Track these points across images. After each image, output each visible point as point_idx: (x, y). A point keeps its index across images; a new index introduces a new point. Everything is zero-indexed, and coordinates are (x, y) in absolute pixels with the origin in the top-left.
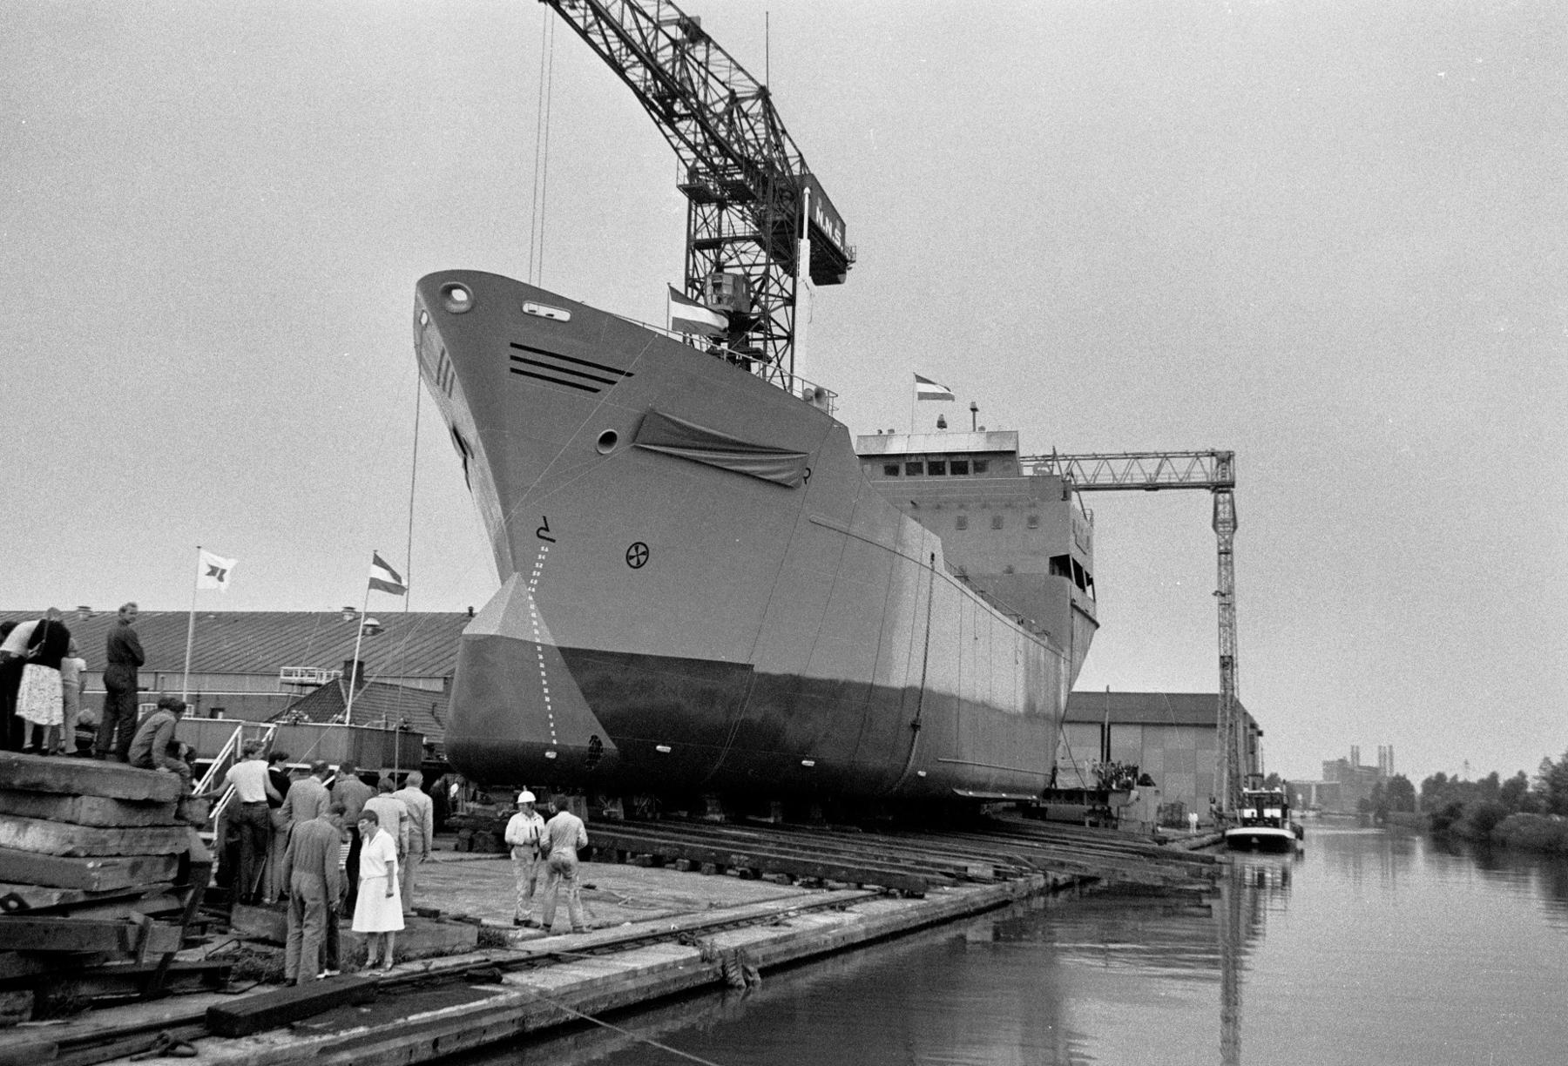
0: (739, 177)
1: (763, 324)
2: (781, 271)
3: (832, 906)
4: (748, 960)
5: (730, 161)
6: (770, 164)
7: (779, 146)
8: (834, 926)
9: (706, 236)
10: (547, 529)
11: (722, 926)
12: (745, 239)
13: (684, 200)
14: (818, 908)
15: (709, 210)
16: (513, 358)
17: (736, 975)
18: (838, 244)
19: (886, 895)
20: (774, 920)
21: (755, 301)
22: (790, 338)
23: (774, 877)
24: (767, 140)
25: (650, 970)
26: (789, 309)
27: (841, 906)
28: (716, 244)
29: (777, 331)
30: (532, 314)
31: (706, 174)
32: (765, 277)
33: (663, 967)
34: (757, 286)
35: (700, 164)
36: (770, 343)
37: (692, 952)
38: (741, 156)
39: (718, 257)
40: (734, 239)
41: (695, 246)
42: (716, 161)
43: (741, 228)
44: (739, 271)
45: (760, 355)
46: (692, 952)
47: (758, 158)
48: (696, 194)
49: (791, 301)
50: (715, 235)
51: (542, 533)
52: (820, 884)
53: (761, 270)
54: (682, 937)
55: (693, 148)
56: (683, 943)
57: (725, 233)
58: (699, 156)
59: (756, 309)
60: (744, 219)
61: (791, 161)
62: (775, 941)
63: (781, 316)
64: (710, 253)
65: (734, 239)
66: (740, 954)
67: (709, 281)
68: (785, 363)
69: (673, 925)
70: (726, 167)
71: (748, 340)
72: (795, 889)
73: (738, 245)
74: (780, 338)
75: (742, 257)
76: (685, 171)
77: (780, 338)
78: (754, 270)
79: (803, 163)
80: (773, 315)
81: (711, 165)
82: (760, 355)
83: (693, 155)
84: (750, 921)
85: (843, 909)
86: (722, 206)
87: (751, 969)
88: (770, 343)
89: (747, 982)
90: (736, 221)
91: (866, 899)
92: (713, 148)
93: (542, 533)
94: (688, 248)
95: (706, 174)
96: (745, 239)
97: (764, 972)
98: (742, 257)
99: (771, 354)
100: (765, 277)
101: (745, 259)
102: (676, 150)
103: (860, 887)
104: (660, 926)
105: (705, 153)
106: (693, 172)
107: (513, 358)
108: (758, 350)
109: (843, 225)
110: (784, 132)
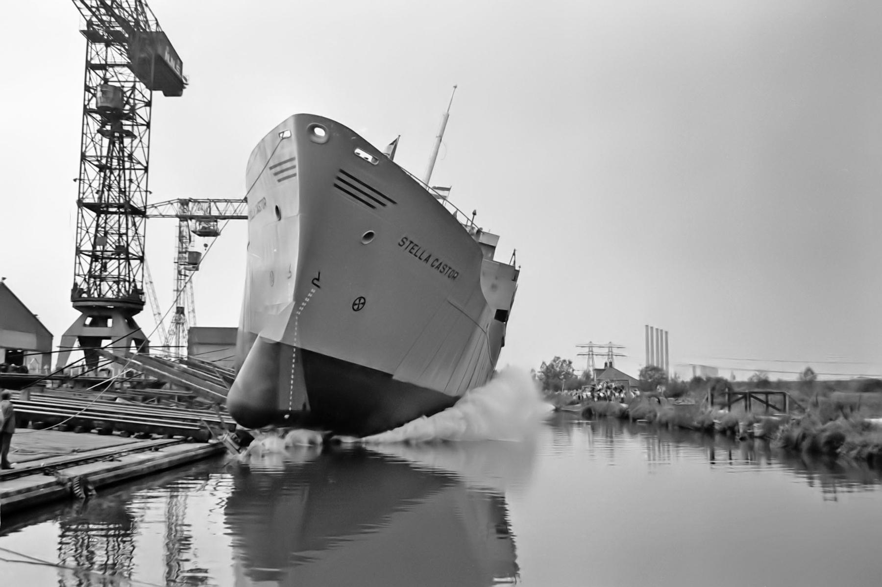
0: (119, 29)
1: (131, 116)
2: (143, 86)
3: (149, 448)
4: (88, 483)
5: (113, 19)
6: (137, 22)
7: (143, 12)
8: (149, 460)
9: (98, 62)
10: (318, 280)
11: (66, 465)
12: (123, 65)
13: (84, 40)
14: (141, 450)
15: (100, 47)
16: (276, 174)
17: (78, 491)
18: (178, 73)
19: (185, 441)
20: (111, 457)
21: (128, 103)
22: (148, 125)
23: (119, 433)
24: (136, 9)
25: (19, 492)
26: (148, 108)
27: (156, 448)
28: (103, 67)
29: (139, 120)
30: (357, 156)
31: (98, 25)
32: (134, 88)
33: (29, 490)
34: (128, 94)
35: (94, 19)
36: (135, 127)
37: (51, 479)
38: (120, 17)
39: (105, 75)
40: (112, 66)
41: (91, 67)
42: (104, 18)
43: (124, 60)
44: (118, 85)
45: (130, 134)
46: (51, 479)
47: (130, 18)
48: (91, 36)
49: (149, 104)
50: (103, 62)
51: (315, 282)
52: (147, 436)
53: (131, 84)
54: (45, 471)
55: (89, 8)
56: (47, 474)
57: (110, 61)
58: (94, 14)
59: (127, 107)
60: (121, 54)
61: (150, 23)
62: (109, 470)
63: (142, 112)
64: (101, 73)
65: (112, 66)
66: (84, 481)
67: (99, 89)
68: (145, 140)
69: (42, 463)
70: (110, 22)
71: (122, 124)
72: (132, 439)
73: (117, 69)
74: (143, 125)
75: (119, 76)
76: (85, 23)
77: (143, 125)
78: (126, 84)
79: (157, 24)
80: (138, 111)
81: (101, 20)
82: (130, 134)
83: (90, 14)
84: (95, 459)
85: (157, 450)
86: (107, 46)
87: (90, 487)
88: (135, 127)
89: (87, 495)
90: (115, 55)
91: (173, 444)
92: (103, 11)
93: (315, 282)
94: (87, 68)
95: (98, 25)
96: (123, 65)
97: (97, 489)
98: (119, 76)
99: (136, 133)
100: (134, 88)
101: (121, 78)
102: (79, 8)
103: (171, 437)
104: (34, 465)
105: (97, 13)
106: (90, 23)
107: (276, 174)
108: (128, 131)
109: (181, 63)
110: (146, 5)
